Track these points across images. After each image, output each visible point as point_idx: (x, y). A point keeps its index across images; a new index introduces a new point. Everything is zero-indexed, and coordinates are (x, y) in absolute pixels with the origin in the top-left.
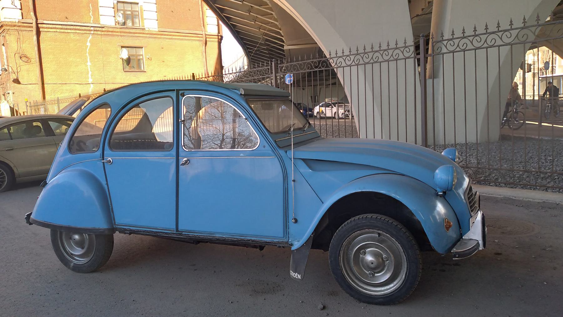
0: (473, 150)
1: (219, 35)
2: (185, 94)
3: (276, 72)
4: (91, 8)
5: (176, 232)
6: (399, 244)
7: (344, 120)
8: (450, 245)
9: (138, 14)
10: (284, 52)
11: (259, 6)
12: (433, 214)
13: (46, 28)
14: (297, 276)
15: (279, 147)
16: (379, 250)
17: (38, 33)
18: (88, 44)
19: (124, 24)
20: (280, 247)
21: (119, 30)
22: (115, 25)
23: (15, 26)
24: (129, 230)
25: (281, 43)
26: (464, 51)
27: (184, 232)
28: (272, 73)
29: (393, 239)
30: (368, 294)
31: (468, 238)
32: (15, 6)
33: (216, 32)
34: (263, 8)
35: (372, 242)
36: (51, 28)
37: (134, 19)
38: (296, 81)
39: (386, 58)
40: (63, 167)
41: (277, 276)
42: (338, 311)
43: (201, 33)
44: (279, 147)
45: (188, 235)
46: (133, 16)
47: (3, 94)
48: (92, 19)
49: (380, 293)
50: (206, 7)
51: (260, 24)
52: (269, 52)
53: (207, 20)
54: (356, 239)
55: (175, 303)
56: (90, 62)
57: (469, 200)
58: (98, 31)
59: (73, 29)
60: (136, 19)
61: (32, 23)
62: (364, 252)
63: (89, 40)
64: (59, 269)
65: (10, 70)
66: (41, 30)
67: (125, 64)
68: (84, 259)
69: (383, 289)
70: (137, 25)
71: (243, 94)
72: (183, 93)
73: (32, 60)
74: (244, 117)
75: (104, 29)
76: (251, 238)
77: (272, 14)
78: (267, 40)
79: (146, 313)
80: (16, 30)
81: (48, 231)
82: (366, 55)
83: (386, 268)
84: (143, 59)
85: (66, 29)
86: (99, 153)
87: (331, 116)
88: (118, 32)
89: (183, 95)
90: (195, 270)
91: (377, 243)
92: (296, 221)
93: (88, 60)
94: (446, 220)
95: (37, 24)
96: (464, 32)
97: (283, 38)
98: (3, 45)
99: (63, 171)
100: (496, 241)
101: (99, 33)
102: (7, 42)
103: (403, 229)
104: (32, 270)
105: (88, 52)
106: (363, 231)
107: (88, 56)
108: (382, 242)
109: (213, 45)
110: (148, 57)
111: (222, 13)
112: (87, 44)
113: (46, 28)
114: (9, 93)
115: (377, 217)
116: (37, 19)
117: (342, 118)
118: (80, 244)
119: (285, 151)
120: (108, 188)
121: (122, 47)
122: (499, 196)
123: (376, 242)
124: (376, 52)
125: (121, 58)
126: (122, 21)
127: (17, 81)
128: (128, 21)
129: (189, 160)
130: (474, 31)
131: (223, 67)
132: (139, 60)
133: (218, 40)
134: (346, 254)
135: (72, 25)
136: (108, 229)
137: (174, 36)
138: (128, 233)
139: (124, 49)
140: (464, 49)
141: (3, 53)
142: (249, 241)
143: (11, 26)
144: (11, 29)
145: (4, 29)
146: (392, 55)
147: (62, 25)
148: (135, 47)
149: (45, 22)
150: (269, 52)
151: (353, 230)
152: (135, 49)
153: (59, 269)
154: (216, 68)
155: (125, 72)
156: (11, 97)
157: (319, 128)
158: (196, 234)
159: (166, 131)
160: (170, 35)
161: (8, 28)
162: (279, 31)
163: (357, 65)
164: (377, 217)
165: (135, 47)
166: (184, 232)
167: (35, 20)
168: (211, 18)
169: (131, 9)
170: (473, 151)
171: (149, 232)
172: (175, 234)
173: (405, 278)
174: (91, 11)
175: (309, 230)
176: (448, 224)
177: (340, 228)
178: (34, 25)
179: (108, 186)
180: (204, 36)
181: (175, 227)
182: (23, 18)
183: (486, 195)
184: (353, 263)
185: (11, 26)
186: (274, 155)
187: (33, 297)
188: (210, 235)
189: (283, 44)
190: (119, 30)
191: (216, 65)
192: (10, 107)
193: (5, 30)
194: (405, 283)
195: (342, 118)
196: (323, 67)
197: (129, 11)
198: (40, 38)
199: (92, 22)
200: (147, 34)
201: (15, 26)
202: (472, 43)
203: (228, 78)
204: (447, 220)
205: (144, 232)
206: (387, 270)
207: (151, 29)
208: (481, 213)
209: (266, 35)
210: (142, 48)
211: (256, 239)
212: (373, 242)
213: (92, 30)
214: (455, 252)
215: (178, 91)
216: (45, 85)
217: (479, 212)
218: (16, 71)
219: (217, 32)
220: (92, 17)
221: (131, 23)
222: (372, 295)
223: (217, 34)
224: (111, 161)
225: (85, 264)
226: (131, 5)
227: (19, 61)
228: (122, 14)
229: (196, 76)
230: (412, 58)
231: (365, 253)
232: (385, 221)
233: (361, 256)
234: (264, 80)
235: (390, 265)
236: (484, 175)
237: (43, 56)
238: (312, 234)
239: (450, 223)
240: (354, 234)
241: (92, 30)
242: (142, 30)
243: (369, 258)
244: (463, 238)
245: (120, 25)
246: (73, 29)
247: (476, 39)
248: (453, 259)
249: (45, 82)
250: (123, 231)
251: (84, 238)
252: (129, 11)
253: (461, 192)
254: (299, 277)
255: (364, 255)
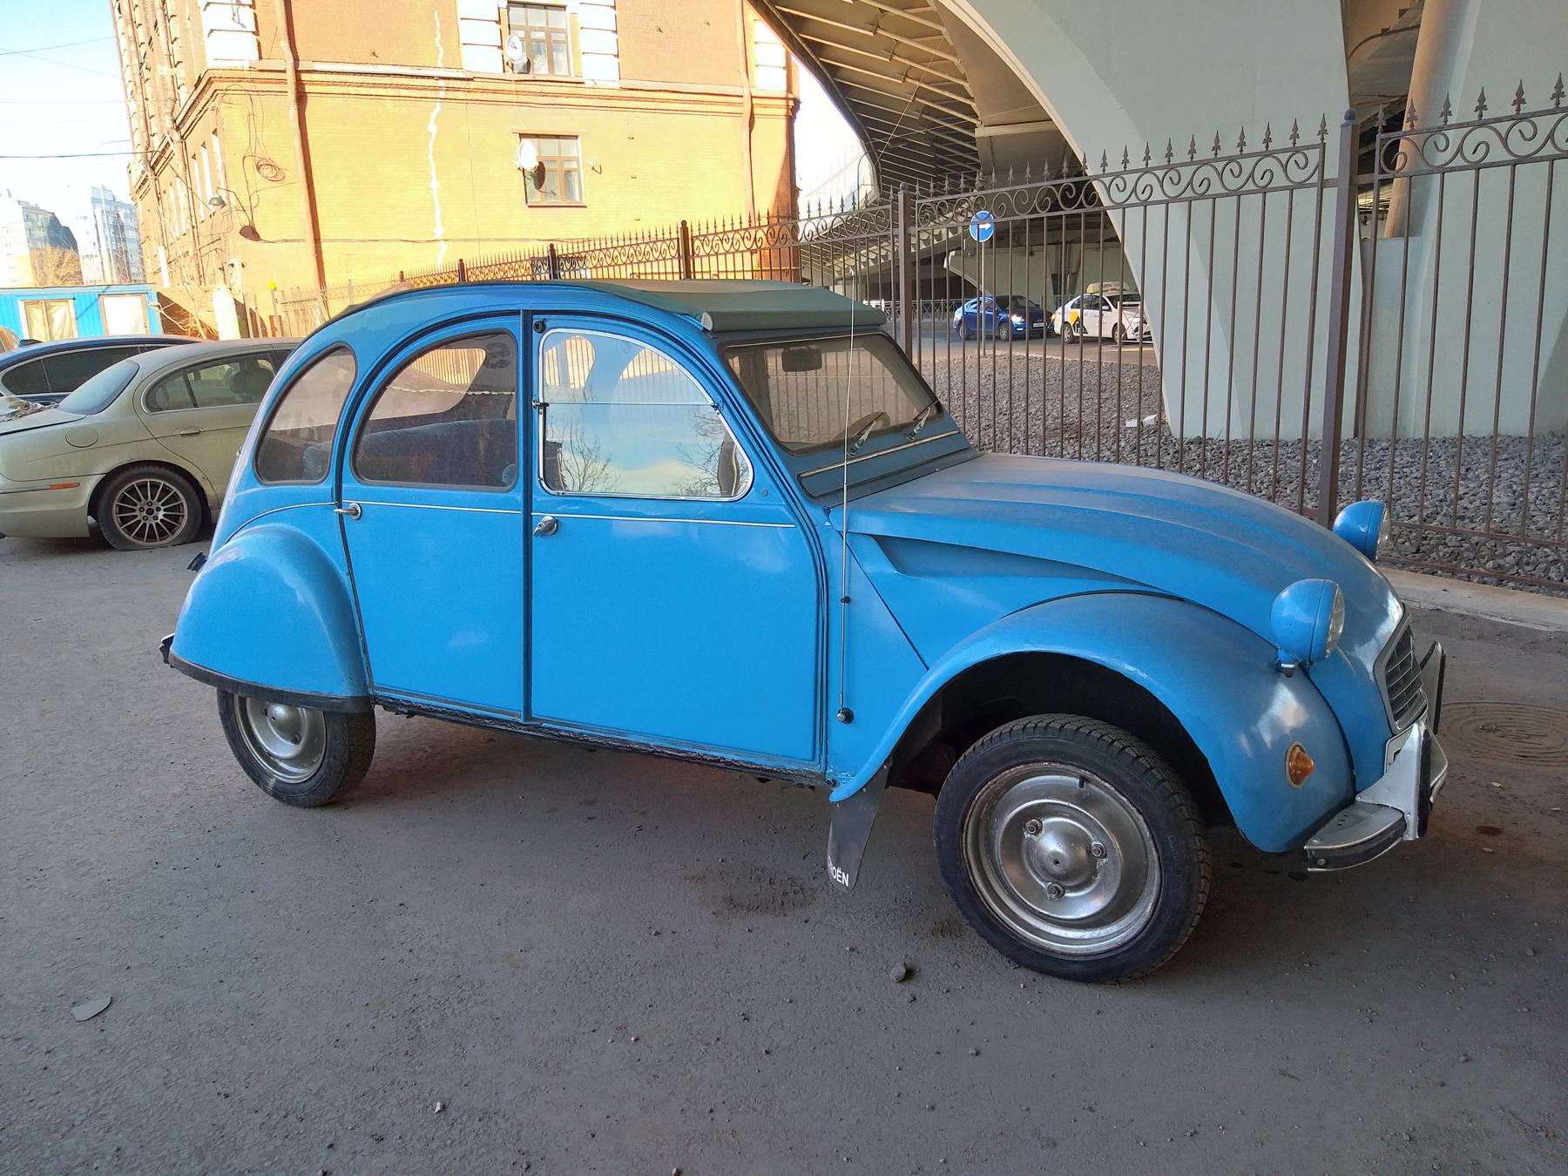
0: (1506, 459)
1: (791, 96)
2: (548, 324)
3: (909, 222)
4: (438, 24)
5: (526, 720)
6: (1140, 813)
7: (1138, 349)
8: (1306, 823)
9: (564, 39)
10: (975, 145)
11: (903, 9)
12: (1254, 729)
13: (322, 83)
14: (840, 876)
15: (810, 495)
16: (1082, 825)
17: (301, 98)
18: (432, 128)
19: (528, 66)
20: (801, 786)
21: (513, 87)
22: (504, 71)
23: (241, 79)
24: (406, 706)
25: (968, 119)
26: (1478, 167)
27: (546, 721)
28: (896, 226)
29: (1122, 798)
30: (1042, 948)
31: (1371, 801)
32: (239, 26)
33: (781, 90)
34: (915, 15)
35: (1058, 799)
36: (334, 84)
37: (554, 53)
38: (1013, 229)
39: (1232, 183)
40: (246, 519)
41: (804, 858)
42: (945, 991)
43: (738, 91)
44: (810, 495)
45: (558, 730)
46: (549, 46)
47: (221, 267)
48: (441, 56)
49: (1078, 947)
50: (752, 14)
51: (908, 62)
52: (934, 144)
53: (756, 54)
54: (1023, 780)
55: (507, 921)
56: (438, 179)
57: (1388, 682)
58: (458, 90)
59: (391, 86)
60: (561, 54)
61: (284, 72)
62: (1036, 826)
63: (433, 115)
64: (244, 790)
65: (234, 202)
66: (308, 88)
67: (531, 184)
68: (301, 771)
69: (1087, 934)
70: (561, 73)
71: (710, 328)
72: (543, 323)
73: (288, 174)
74: (711, 402)
75: (472, 85)
76: (725, 756)
77: (940, 33)
78: (928, 110)
79: (422, 948)
80: (243, 92)
81: (211, 693)
82: (1173, 174)
83: (1099, 877)
84: (577, 170)
85: (374, 85)
86: (328, 486)
87: (1097, 335)
88: (510, 92)
89: (540, 327)
90: (589, 818)
91: (1075, 804)
92: (849, 717)
93: (434, 174)
94: (1294, 749)
95: (297, 73)
96: (1481, 107)
97: (973, 105)
98: (215, 132)
99: (243, 532)
100: (1494, 784)
101: (460, 95)
102: (224, 126)
103: (1153, 771)
104: (177, 790)
105: (431, 150)
106: (1036, 766)
107: (432, 162)
108: (1088, 801)
109: (771, 129)
110: (591, 163)
111: (797, 34)
112: (430, 129)
113: (322, 83)
114: (232, 265)
115: (1079, 728)
116: (296, 59)
117: (1132, 343)
118: (290, 730)
119: (824, 509)
120: (354, 586)
121: (522, 136)
122: (1544, 629)
123: (1072, 803)
124: (1204, 163)
125: (519, 169)
126: (521, 61)
127: (250, 233)
128: (539, 59)
129: (557, 521)
130: (1514, 105)
131: (799, 189)
132: (568, 173)
133: (788, 112)
134: (985, 827)
135: (389, 75)
136: (354, 699)
137: (663, 101)
138: (403, 713)
139: (525, 141)
140: (1476, 163)
141: (216, 155)
142: (718, 761)
143: (231, 79)
144: (231, 88)
145: (216, 90)
146: (1252, 175)
147: (361, 74)
148: (558, 137)
149: (318, 67)
150: (934, 144)
151: (1006, 761)
152: (557, 140)
153: (244, 790)
154: (778, 194)
155: (530, 207)
156: (237, 275)
157: (1060, 375)
158: (578, 730)
159: (637, 374)
160: (654, 100)
161: (224, 86)
162: (961, 83)
163: (1145, 204)
164: (1079, 728)
165: (558, 137)
166: (546, 721)
167: (291, 60)
168: (768, 46)
169: (545, 26)
170: (1506, 462)
171: (456, 715)
172: (521, 724)
173: (1152, 915)
174: (437, 32)
175: (877, 750)
176: (1300, 765)
177: (967, 753)
178: (290, 76)
179: (352, 579)
180: (747, 100)
181: (520, 706)
182: (261, 58)
183: (1503, 621)
184: (1002, 855)
185: (233, 81)
186: (793, 520)
187: (155, 871)
188: (615, 737)
189: (974, 121)
190: (513, 87)
191: (779, 186)
192: (236, 302)
193: (218, 92)
194: (1150, 929)
195: (1132, 343)
196: (1043, 208)
197: (541, 29)
198: (307, 113)
199: (440, 65)
200: (590, 97)
201: (241, 79)
202: (1504, 141)
203: (776, 235)
204: (1298, 750)
205: (443, 712)
206: (1100, 885)
207: (600, 84)
208: (1419, 730)
209: (921, 93)
210: (577, 137)
211: (736, 758)
212: (1062, 800)
213: (440, 88)
214: (1317, 850)
215: (529, 314)
216: (324, 245)
217: (1415, 726)
218: (246, 204)
219: (784, 87)
220: (441, 49)
221: (546, 66)
222: (1052, 951)
223: (783, 95)
224: (357, 511)
225: (303, 785)
226: (547, 13)
227: (254, 176)
228: (522, 39)
229: (692, 231)
230: (1312, 185)
231: (1037, 830)
232: (1100, 741)
233: (1027, 836)
234: (887, 241)
235: (1111, 869)
236: (1517, 549)
237: (314, 163)
238: (885, 764)
239: (1306, 761)
240: (1007, 771)
241: (440, 88)
242: (575, 85)
243: (1050, 844)
244: (1358, 798)
245: (516, 71)
246: (391, 86)
247: (1520, 131)
248: (1309, 869)
249: (323, 236)
250: (392, 705)
251: (299, 715)
252: (541, 29)
253: (1368, 656)
254: (846, 880)
255: (1036, 834)
